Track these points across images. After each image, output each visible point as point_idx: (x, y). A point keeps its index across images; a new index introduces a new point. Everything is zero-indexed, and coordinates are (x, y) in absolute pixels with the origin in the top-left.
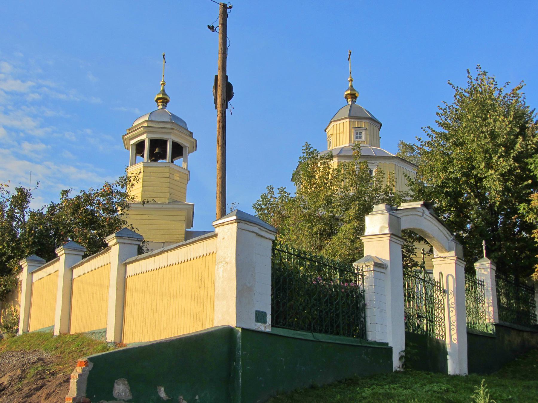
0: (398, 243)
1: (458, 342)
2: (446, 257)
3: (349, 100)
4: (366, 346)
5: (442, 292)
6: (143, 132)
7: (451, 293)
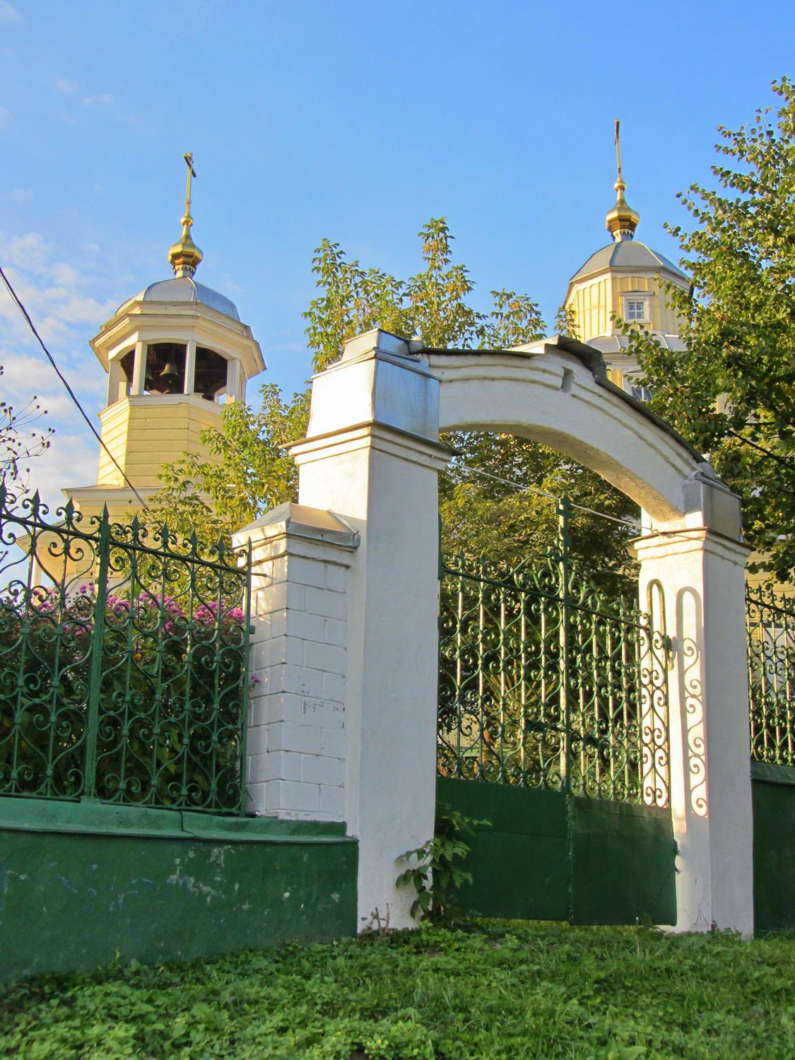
0: (415, 462)
1: (710, 811)
2: (674, 533)
3: (617, 233)
4: (194, 840)
5: (659, 645)
6: (128, 329)
7: (689, 648)
